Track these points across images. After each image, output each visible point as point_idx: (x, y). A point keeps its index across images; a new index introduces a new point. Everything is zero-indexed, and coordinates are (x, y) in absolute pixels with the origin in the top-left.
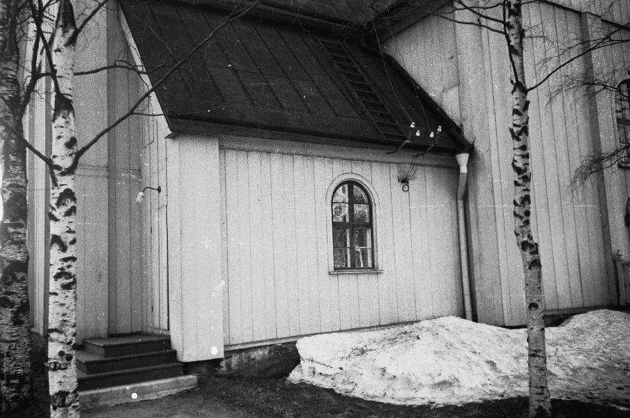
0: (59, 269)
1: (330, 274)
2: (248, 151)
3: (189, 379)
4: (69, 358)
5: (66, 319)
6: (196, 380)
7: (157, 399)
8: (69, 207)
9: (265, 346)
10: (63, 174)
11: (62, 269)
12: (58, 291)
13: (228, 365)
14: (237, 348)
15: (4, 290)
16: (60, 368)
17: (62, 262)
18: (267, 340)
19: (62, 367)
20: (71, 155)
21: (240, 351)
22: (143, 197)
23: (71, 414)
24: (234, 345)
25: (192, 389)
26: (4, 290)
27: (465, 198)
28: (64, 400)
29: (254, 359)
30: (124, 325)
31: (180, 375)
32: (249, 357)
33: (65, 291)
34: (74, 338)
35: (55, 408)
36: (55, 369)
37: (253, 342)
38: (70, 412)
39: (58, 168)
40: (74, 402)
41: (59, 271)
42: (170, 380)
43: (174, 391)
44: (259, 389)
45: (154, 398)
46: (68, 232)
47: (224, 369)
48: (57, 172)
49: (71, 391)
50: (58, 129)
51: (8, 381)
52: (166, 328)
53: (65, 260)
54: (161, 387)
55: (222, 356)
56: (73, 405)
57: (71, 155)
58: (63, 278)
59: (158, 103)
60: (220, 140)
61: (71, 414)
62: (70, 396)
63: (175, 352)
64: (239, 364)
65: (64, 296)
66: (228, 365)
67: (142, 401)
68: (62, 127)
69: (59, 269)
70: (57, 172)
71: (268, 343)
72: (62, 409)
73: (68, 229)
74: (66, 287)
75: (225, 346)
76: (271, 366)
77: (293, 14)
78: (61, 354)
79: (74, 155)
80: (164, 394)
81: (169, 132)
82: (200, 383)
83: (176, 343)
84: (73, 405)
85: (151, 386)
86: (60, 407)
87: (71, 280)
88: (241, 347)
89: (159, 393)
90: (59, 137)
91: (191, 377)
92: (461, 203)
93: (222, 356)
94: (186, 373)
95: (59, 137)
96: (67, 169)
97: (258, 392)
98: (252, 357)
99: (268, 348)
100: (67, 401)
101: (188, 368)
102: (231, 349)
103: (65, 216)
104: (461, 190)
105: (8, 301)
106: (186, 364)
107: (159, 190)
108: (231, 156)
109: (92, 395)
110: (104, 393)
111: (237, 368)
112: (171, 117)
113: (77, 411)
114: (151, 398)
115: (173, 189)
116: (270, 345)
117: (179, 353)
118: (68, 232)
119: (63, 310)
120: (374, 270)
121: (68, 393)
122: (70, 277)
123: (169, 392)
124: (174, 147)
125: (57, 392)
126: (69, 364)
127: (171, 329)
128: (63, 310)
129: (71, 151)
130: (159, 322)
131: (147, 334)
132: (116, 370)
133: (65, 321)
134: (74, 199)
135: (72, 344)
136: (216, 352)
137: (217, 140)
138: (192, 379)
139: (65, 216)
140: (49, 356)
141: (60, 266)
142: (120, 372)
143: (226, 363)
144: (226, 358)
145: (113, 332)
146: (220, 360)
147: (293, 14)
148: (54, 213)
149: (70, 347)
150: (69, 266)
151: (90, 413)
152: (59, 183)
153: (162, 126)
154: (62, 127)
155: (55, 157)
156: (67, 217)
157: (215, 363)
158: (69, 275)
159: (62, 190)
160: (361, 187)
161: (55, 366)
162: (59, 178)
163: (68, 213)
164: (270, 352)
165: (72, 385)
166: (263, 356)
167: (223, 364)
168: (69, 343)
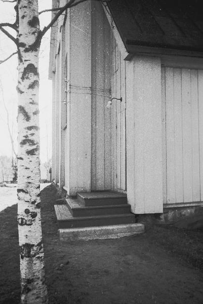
0: (24, 137)
2: (181, 68)
3: (138, 227)
4: (34, 215)
5: (30, 181)
6: (143, 228)
7: (116, 239)
8: (32, 81)
9: (192, 207)
10: (26, 51)
11: (26, 137)
12: (22, 156)
13: (166, 218)
14: (172, 206)
16: (26, 224)
17: (27, 130)
18: (193, 203)
19: (28, 223)
20: (34, 33)
21: (175, 208)
22: (111, 104)
23: (35, 264)
24: (170, 204)
25: (141, 234)
28: (29, 252)
29: (184, 215)
30: (100, 184)
31: (133, 223)
32: (181, 213)
33: (30, 156)
34: (39, 198)
35: (22, 258)
36: (22, 224)
37: (183, 203)
38: (34, 262)
39: (23, 45)
40: (38, 254)
41: (24, 138)
42: (124, 226)
43: (128, 234)
44: (191, 241)
45: (115, 238)
46: (31, 103)
47: (163, 220)
48: (22, 49)
49: (36, 244)
50: (22, 9)
52: (124, 189)
53: (30, 128)
54: (118, 230)
55: (161, 211)
56: (36, 256)
57: (34, 33)
58: (28, 144)
59: (120, 38)
60: (162, 60)
61: (35, 264)
62: (35, 248)
63: (130, 206)
64: (174, 217)
65: (28, 160)
66: (166, 218)
67: (107, 239)
68: (25, 7)
69: (24, 137)
71: (194, 205)
72: (27, 259)
73: (31, 101)
74: (31, 153)
75: (164, 205)
76: (197, 222)
78: (27, 211)
79: (36, 34)
80: (121, 235)
81: (127, 54)
82: (146, 229)
83: (131, 199)
84: (38, 256)
85: (113, 230)
86: (26, 257)
87: (34, 147)
88: (175, 206)
89: (119, 234)
90: (23, 17)
91: (140, 225)
93: (161, 211)
94: (136, 222)
95: (23, 17)
96: (30, 46)
97: (190, 243)
98: (183, 213)
99: (194, 208)
100: (32, 253)
101: (138, 218)
102: (168, 207)
103: (28, 89)
106: (137, 215)
107: (121, 100)
108: (169, 74)
109: (74, 232)
110: (82, 232)
111: (172, 220)
112: (128, 44)
113: (41, 261)
114: (112, 238)
115: (130, 100)
116: (196, 206)
117: (132, 208)
118: (31, 103)
119: (27, 173)
121: (33, 245)
122: (34, 144)
123: (125, 235)
124: (130, 66)
125: (24, 244)
126: (34, 220)
127: (127, 190)
128: (27, 173)
129: (34, 29)
130: (119, 184)
131: (115, 192)
132: (90, 216)
133: (30, 183)
134: (36, 74)
135: (36, 203)
136: (160, 210)
137: (159, 61)
138: (141, 227)
139: (28, 89)
140: (18, 213)
141: (25, 134)
142: (94, 217)
143: (164, 216)
144: (164, 213)
145: (94, 189)
146: (160, 214)
149: (34, 206)
150: (32, 134)
151: (72, 244)
153: (122, 50)
154: (25, 7)
156: (30, 90)
157: (157, 215)
158: (32, 143)
161: (22, 222)
162: (23, 54)
164: (196, 211)
165: (36, 239)
166: (191, 213)
167: (162, 217)
168: (33, 203)
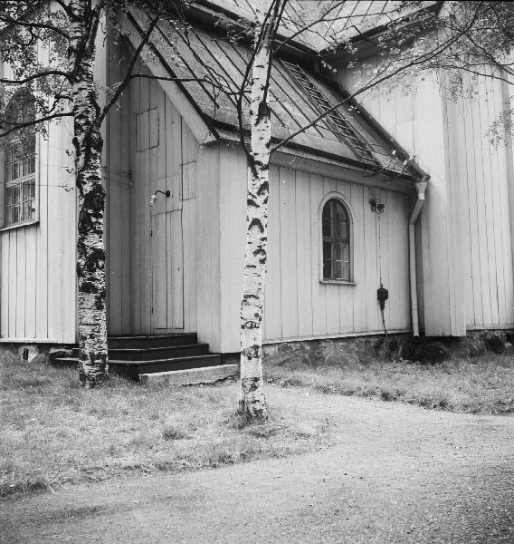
1: (320, 282)
10: (263, 169)
11: (260, 246)
15: (88, 276)
26: (88, 276)
27: (418, 223)
39: (259, 163)
51: (92, 361)
63: (207, 346)
70: (258, 167)
77: (214, 14)
92: (412, 228)
104: (414, 216)
105: (93, 286)
107: (168, 194)
120: (351, 283)
147: (214, 14)
148: (254, 200)
152: (259, 176)
155: (255, 154)
159: (262, 182)
160: (342, 205)
162: (259, 172)
163: (266, 202)
